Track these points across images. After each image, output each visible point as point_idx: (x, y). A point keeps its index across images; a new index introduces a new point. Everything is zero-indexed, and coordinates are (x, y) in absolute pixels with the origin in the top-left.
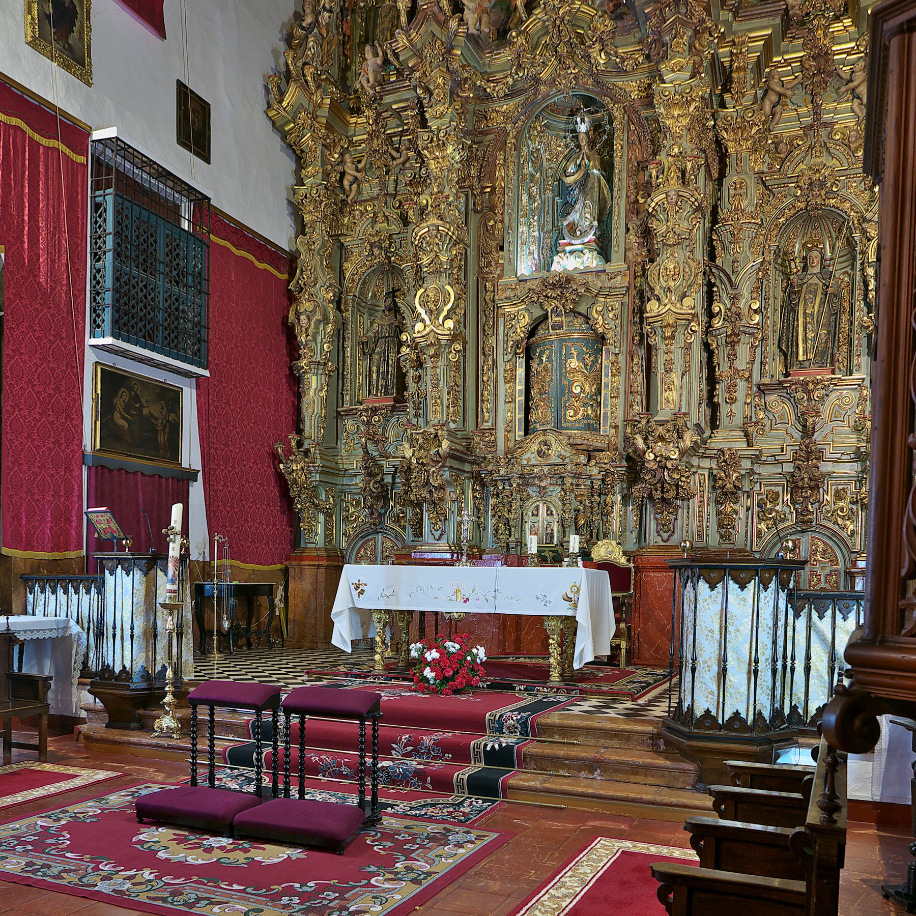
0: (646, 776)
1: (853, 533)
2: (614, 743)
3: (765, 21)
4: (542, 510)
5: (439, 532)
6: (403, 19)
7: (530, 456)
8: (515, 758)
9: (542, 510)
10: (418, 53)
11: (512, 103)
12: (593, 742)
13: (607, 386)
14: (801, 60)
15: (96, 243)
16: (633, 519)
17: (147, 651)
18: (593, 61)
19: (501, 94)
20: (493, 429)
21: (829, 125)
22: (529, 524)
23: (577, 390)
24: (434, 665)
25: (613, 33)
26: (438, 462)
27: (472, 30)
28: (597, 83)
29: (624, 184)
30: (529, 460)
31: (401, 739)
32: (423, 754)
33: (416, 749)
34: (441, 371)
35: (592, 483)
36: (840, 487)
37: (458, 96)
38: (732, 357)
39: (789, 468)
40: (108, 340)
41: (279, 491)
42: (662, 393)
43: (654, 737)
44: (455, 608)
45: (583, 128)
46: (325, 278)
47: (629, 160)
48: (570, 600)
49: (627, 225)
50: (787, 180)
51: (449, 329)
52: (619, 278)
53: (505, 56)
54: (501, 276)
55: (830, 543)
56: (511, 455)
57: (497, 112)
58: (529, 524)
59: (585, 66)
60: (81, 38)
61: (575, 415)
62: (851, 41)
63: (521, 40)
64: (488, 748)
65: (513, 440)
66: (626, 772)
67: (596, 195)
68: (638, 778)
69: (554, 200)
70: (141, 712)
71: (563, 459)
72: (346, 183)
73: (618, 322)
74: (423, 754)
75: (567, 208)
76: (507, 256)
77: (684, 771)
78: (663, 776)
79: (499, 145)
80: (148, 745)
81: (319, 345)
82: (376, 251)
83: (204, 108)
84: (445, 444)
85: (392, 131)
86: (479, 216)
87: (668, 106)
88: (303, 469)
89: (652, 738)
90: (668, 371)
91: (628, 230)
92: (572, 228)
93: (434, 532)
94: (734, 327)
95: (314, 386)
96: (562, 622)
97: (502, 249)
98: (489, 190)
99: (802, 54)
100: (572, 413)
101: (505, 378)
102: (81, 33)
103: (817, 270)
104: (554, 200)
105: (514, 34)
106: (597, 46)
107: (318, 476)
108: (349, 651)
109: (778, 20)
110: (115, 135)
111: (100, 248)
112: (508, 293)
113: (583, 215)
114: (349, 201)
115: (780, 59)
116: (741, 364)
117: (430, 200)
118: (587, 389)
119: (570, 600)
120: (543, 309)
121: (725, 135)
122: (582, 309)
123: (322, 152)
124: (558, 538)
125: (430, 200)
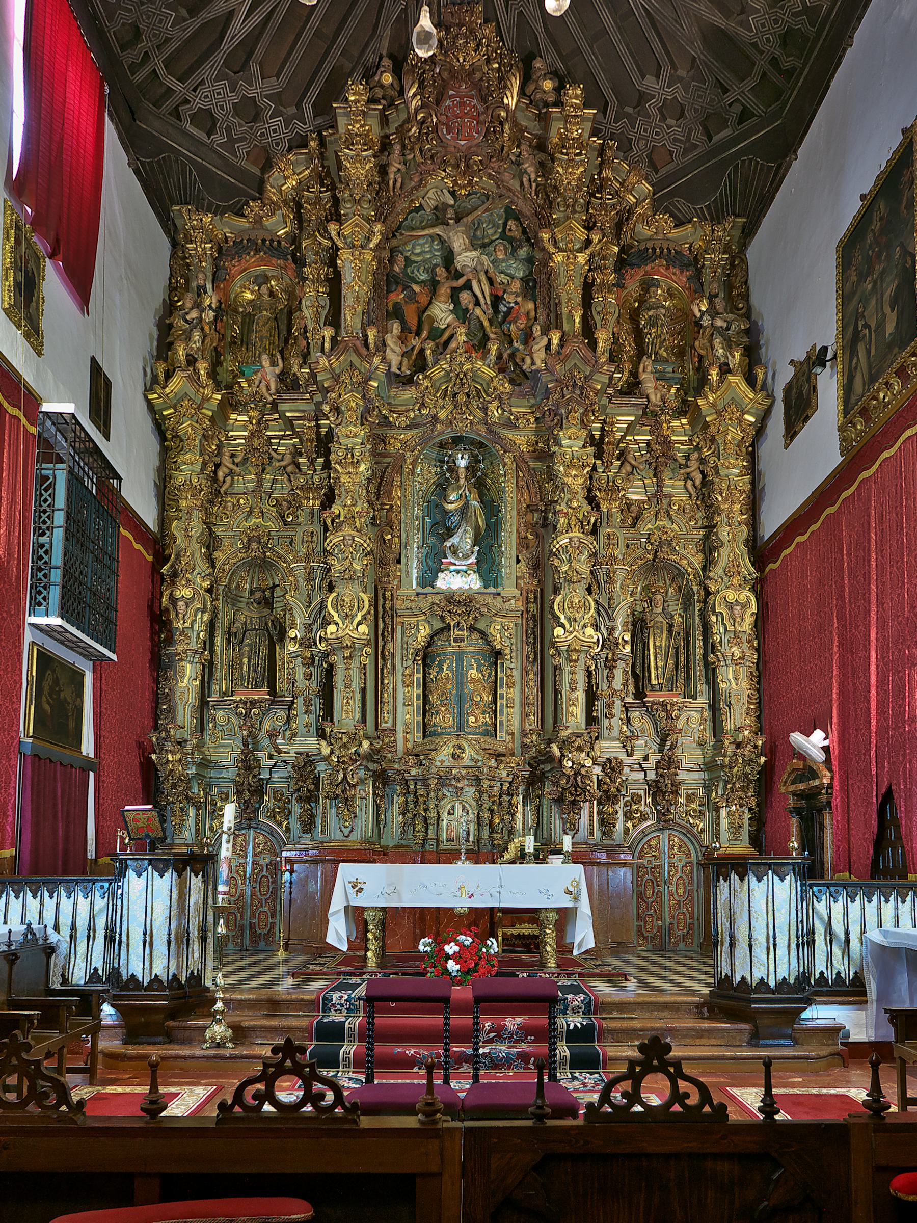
0: (709, 1038)
1: (703, 831)
2: (666, 1014)
3: (631, 410)
4: (459, 810)
5: (349, 829)
6: (327, 345)
7: (443, 756)
8: (596, 1034)
9: (459, 810)
10: (336, 378)
11: (410, 433)
12: (647, 1015)
13: (502, 697)
14: (648, 443)
15: (40, 517)
16: (531, 818)
17: (178, 958)
18: (489, 413)
19: (404, 425)
20: (393, 730)
21: (670, 496)
22: (445, 823)
23: (477, 699)
24: (456, 957)
25: (510, 395)
26: (356, 761)
27: (394, 369)
28: (490, 431)
29: (515, 520)
30: (442, 762)
31: (484, 1026)
32: (505, 1039)
33: (499, 1034)
34: (354, 673)
35: (501, 785)
36: (690, 792)
37: (367, 421)
38: (610, 678)
39: (652, 775)
40: (55, 621)
41: (142, 782)
42: (567, 709)
43: (699, 1006)
44: (462, 904)
45: (462, 463)
46: (202, 566)
47: (519, 502)
48: (570, 893)
49: (517, 557)
50: (639, 536)
51: (364, 634)
52: (513, 602)
53: (409, 394)
54: (399, 587)
55: (685, 839)
56: (419, 755)
57: (396, 439)
58: (445, 823)
59: (480, 414)
60: (38, 309)
61: (476, 722)
62: (686, 435)
63: (426, 383)
64: (572, 1027)
65: (411, 741)
66: (693, 1037)
67: (473, 522)
68: (704, 1041)
69: (424, 519)
70: (172, 1023)
71: (476, 761)
72: (221, 474)
73: (513, 640)
74: (505, 1039)
75: (450, 533)
76: (404, 569)
77: (740, 1031)
78: (723, 1037)
79: (397, 469)
80: (204, 1057)
81: (195, 633)
82: (254, 545)
83: (108, 384)
84: (366, 744)
85: (273, 433)
86: (377, 529)
87: (570, 466)
88: (180, 760)
89: (697, 1007)
90: (573, 689)
91: (518, 561)
92: (454, 551)
93: (342, 828)
94: (614, 654)
95: (187, 678)
96: (557, 913)
97: (399, 562)
98: (388, 507)
99: (649, 438)
100: (474, 720)
101: (404, 682)
102: (38, 303)
103: (660, 610)
104: (424, 519)
105: (421, 377)
106: (495, 403)
107: (194, 768)
108: (345, 948)
109: (641, 412)
110: (72, 411)
111: (44, 522)
112: (407, 604)
113: (463, 539)
114: (222, 492)
115: (631, 438)
116: (617, 684)
117: (342, 511)
118: (485, 699)
119: (570, 893)
120: (444, 622)
121: (598, 494)
122: (481, 626)
123: (200, 442)
124: (475, 835)
125: (342, 511)
